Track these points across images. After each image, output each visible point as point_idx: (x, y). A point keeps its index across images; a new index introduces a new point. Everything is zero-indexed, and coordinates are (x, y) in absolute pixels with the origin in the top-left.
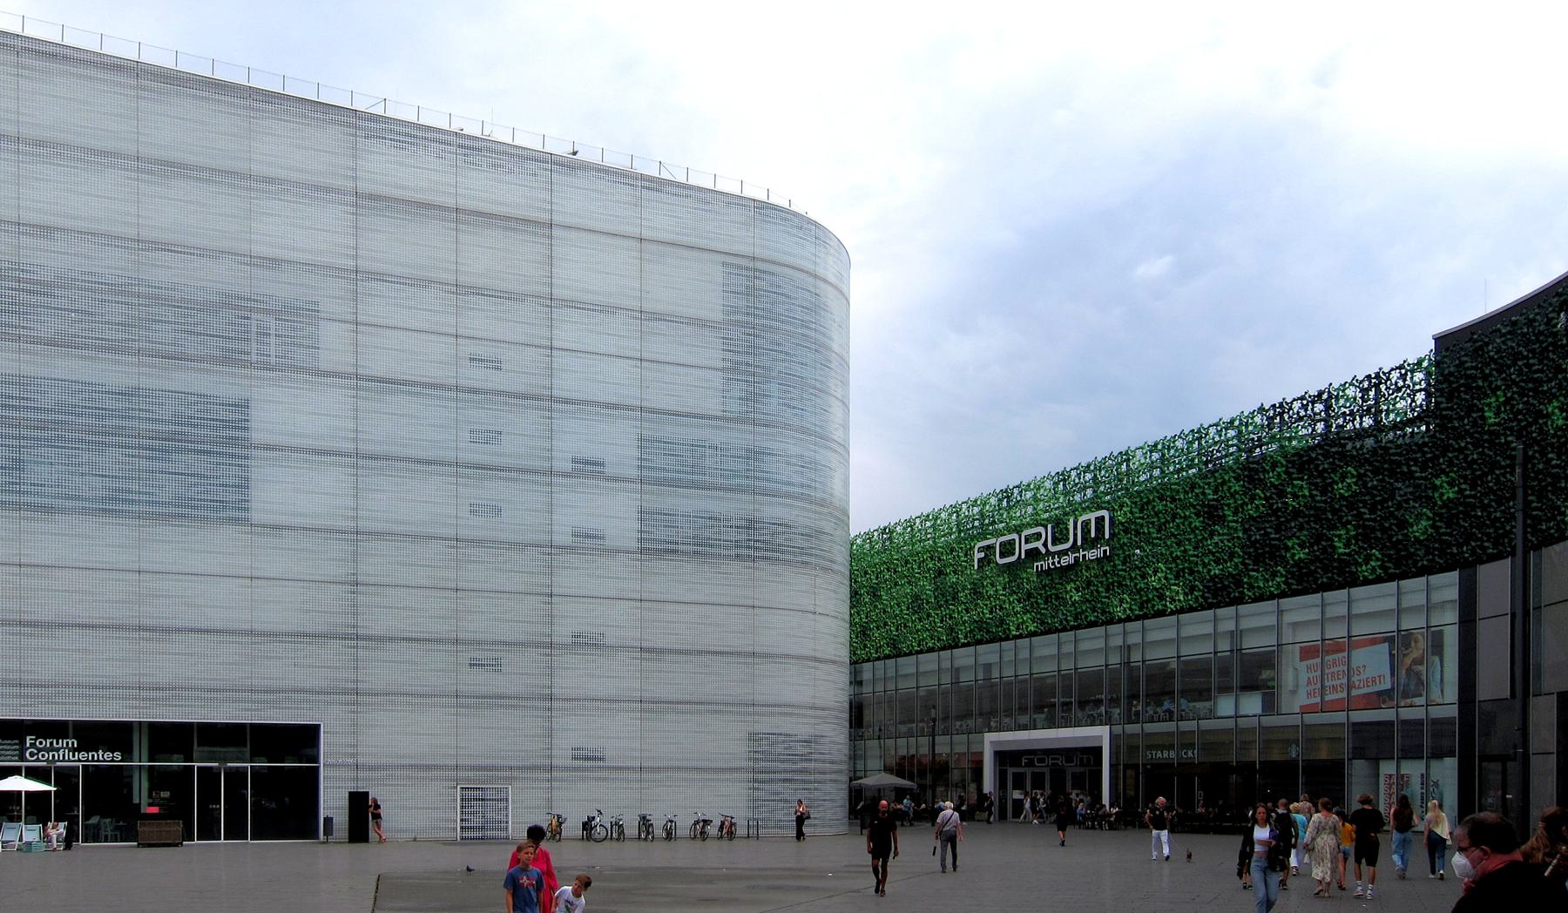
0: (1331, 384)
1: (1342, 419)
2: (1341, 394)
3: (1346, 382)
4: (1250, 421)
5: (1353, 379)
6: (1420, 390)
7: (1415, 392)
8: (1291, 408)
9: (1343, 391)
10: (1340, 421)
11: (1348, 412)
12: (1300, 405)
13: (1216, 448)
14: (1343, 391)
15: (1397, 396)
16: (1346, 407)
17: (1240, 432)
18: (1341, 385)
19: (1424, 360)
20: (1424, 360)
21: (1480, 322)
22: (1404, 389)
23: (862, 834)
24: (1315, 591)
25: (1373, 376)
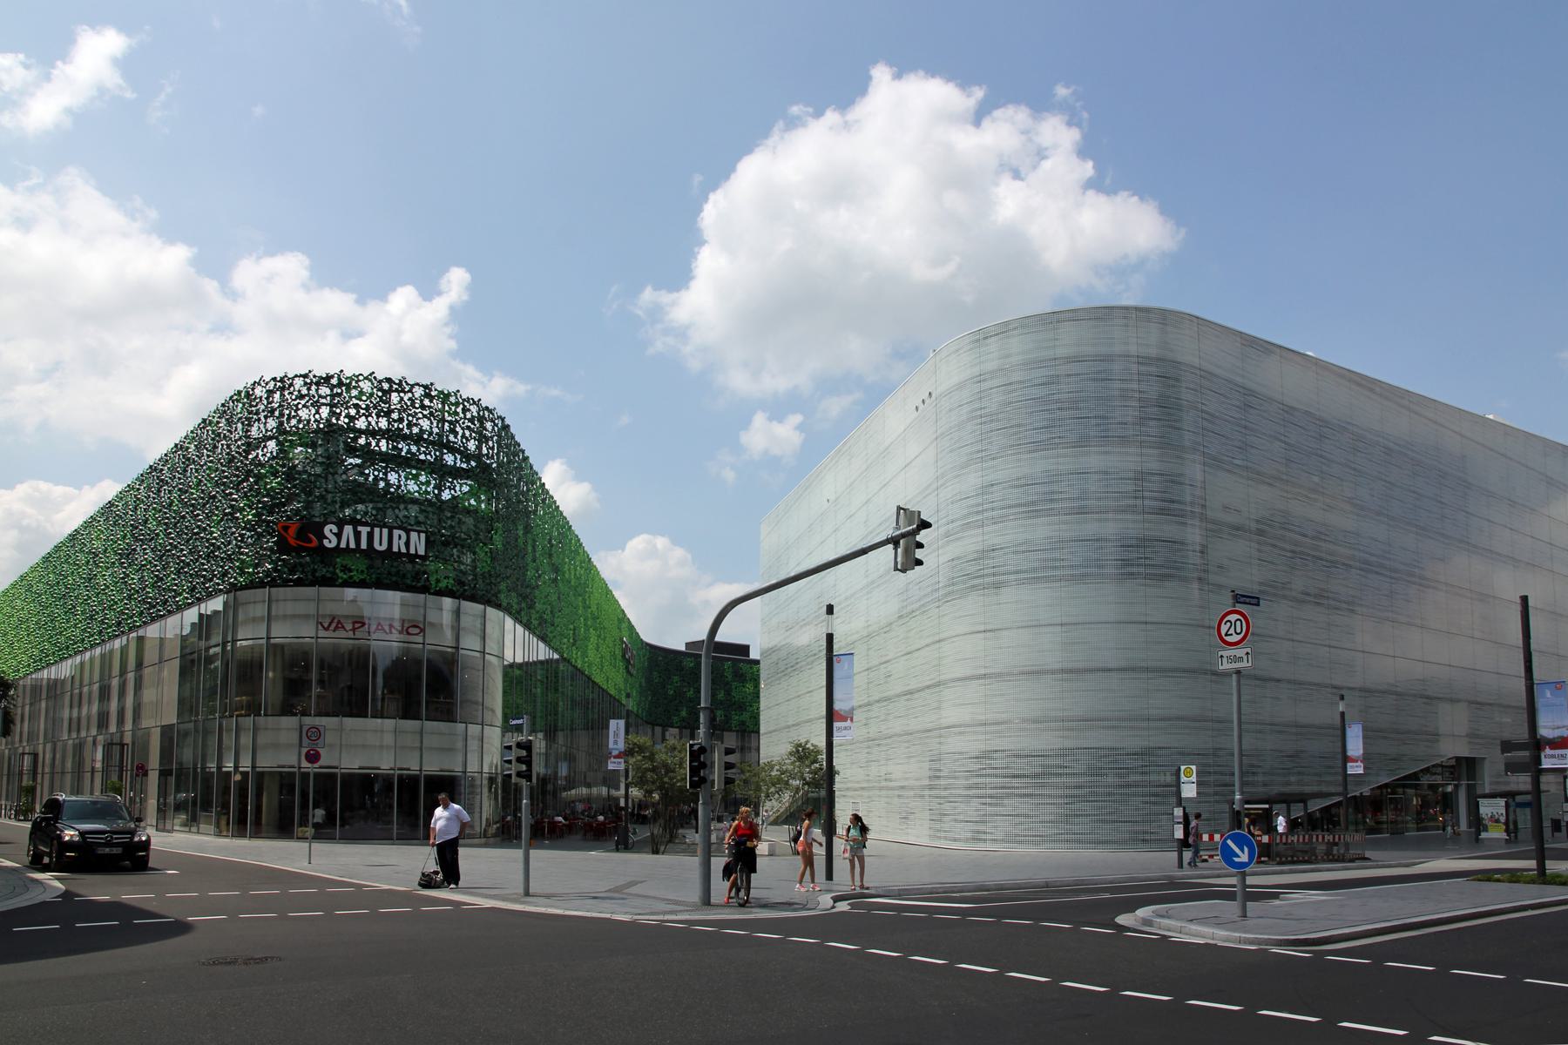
0: (373, 373)
4: (354, 384)
5: (371, 375)
8: (291, 385)
10: (353, 412)
12: (302, 383)
13: (303, 402)
18: (354, 375)
19: (332, 377)
20: (332, 377)
22: (307, 398)
24: (312, 584)
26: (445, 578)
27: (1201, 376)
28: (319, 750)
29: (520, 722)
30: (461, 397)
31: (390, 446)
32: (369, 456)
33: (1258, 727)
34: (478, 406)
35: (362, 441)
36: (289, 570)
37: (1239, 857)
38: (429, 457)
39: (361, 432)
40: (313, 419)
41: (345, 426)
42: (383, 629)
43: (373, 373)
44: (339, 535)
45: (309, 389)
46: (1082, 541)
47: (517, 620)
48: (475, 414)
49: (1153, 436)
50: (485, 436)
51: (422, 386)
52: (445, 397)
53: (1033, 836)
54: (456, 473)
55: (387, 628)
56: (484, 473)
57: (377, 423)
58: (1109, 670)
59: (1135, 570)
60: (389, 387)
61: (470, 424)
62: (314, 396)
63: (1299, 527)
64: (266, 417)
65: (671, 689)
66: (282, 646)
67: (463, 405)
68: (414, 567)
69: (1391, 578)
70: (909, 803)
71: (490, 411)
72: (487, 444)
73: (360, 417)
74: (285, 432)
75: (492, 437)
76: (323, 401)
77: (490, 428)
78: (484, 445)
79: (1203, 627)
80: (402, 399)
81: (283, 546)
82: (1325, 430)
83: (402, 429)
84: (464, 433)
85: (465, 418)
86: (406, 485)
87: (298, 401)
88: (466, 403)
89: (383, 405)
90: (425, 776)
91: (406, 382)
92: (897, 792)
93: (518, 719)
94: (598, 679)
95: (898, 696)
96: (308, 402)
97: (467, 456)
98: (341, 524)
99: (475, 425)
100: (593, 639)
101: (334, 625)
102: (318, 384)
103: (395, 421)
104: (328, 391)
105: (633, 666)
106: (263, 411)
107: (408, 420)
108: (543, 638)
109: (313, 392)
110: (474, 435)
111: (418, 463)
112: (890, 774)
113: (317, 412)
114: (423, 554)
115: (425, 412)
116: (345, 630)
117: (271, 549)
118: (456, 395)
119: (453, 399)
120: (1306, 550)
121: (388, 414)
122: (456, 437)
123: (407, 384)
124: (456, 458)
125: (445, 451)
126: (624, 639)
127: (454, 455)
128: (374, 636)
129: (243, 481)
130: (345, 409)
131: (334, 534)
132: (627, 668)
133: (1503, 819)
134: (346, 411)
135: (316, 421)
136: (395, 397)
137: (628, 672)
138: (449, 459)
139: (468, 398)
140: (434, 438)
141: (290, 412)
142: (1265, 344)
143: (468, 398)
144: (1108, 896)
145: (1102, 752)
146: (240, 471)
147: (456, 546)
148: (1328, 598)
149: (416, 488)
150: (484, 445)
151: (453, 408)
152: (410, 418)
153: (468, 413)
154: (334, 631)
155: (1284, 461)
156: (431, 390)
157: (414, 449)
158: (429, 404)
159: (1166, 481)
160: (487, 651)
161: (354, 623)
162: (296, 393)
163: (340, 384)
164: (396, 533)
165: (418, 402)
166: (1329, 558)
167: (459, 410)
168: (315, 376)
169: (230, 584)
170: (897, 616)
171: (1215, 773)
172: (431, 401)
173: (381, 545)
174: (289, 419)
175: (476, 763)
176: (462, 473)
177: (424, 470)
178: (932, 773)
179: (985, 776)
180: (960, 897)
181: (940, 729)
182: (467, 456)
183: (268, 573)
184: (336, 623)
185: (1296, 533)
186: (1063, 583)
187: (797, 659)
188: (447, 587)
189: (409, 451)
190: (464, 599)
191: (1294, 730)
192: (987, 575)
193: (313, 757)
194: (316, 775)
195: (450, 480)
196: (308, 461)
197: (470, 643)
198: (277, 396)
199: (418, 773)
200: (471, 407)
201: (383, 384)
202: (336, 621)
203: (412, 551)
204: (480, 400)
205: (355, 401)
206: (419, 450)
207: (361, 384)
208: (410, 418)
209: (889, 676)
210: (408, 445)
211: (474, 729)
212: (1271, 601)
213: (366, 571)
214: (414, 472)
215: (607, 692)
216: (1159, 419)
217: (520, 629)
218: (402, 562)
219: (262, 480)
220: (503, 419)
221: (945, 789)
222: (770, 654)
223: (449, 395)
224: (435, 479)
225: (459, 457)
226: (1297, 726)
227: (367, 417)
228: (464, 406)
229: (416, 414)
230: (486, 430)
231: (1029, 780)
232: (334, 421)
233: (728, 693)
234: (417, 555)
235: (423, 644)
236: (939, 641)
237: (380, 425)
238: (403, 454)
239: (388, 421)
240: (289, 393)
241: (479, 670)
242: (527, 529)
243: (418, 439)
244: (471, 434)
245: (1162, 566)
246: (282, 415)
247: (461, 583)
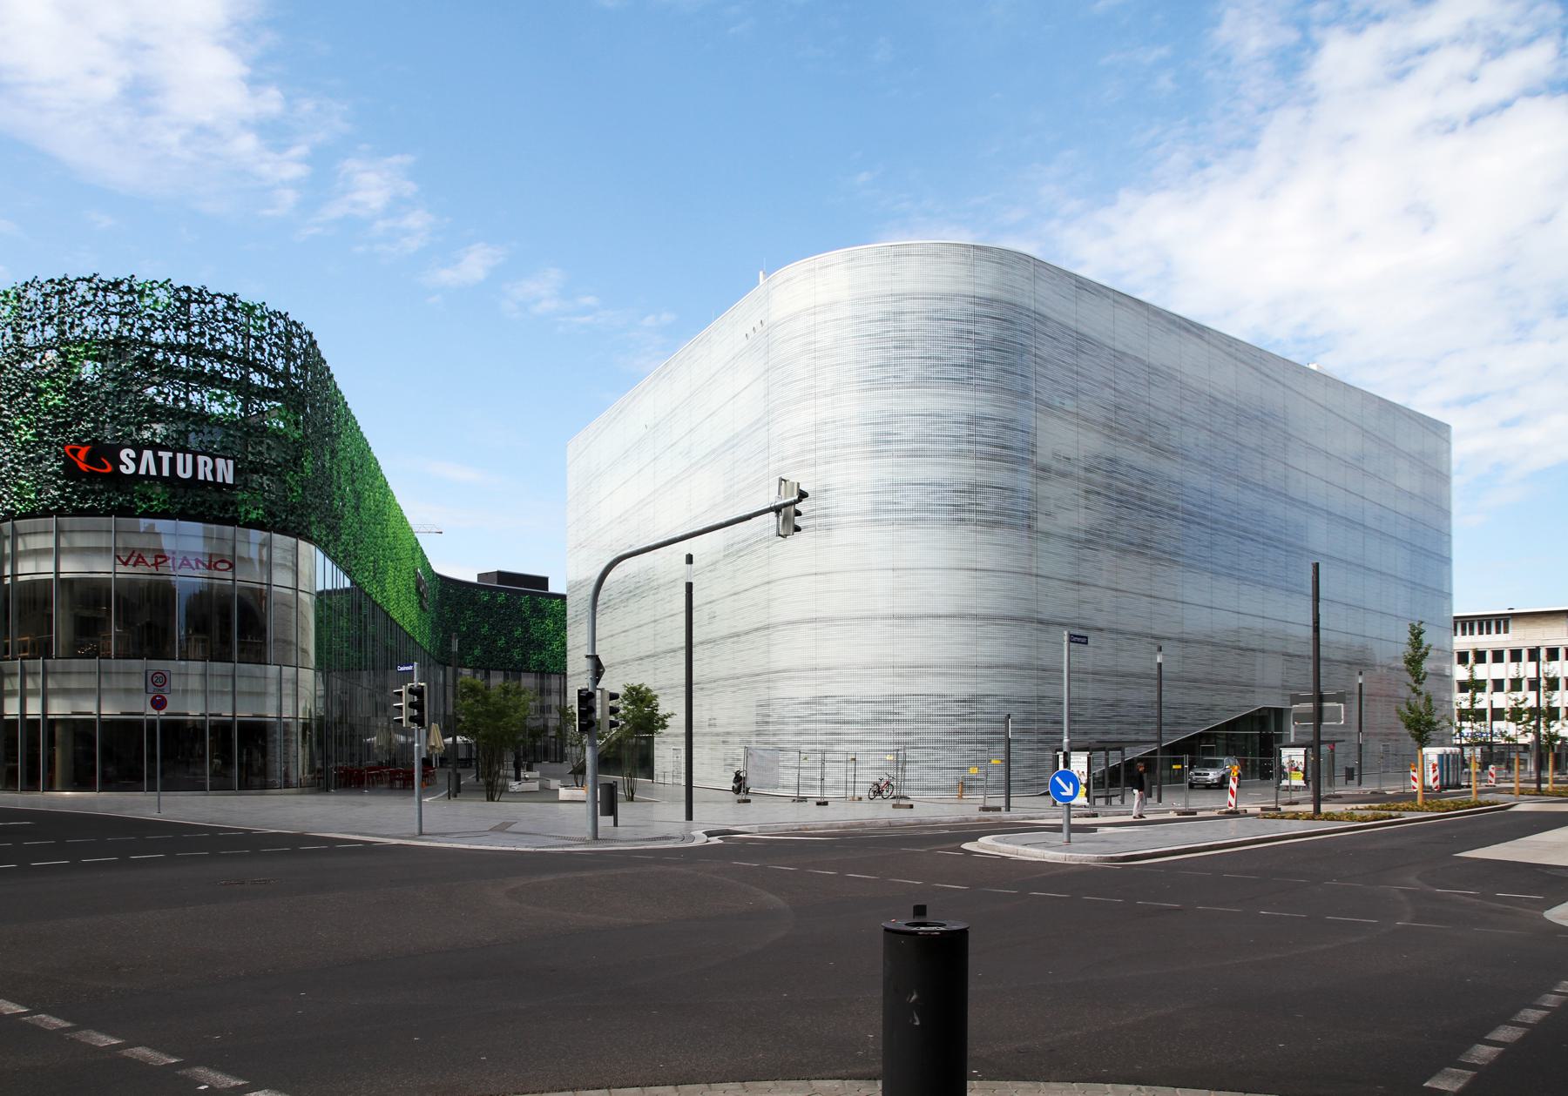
0: (169, 280)
1: (197, 331)
5: (166, 282)
10: (147, 323)
13: (88, 309)
15: (223, 326)
19: (122, 282)
21: (1335, 380)
22: (93, 306)
24: (108, 514)
26: (255, 509)
27: (1035, 319)
28: (166, 696)
29: (410, 668)
30: (267, 310)
31: (191, 363)
32: (170, 373)
33: (1081, 676)
34: (285, 321)
35: (159, 356)
36: (79, 497)
37: (1065, 791)
38: (234, 376)
39: (157, 346)
40: (101, 330)
41: (139, 339)
42: (189, 564)
43: (169, 280)
44: (137, 461)
45: (95, 295)
46: (915, 484)
47: (327, 554)
48: (282, 329)
49: (988, 380)
51: (225, 297)
52: (249, 310)
54: (264, 394)
55: (193, 563)
56: (292, 394)
57: (175, 336)
58: (939, 616)
59: (966, 515)
60: (186, 298)
61: (277, 340)
62: (101, 304)
63: (1126, 476)
64: (43, 324)
65: (464, 625)
66: (71, 581)
67: (270, 319)
68: (221, 496)
69: (1212, 529)
70: (735, 749)
71: (298, 327)
72: (295, 362)
73: (156, 329)
74: (67, 343)
75: (300, 355)
76: (113, 309)
77: (298, 345)
78: (292, 363)
79: (1031, 575)
80: (203, 311)
81: (70, 470)
82: (1154, 377)
83: (204, 344)
84: (271, 350)
85: (272, 333)
86: (209, 407)
87: (82, 308)
88: (272, 317)
89: (181, 317)
90: (239, 722)
91: (206, 291)
92: (721, 739)
93: (408, 665)
94: (395, 615)
95: (723, 638)
96: (94, 309)
97: (275, 376)
98: (139, 448)
99: (283, 341)
100: (391, 573)
101: (134, 559)
102: (105, 290)
103: (195, 335)
104: (117, 299)
105: (426, 599)
106: (39, 317)
107: (210, 334)
108: (348, 573)
109: (100, 299)
110: (281, 352)
111: (223, 383)
112: (715, 719)
113: (106, 322)
114: (232, 482)
115: (229, 327)
116: (147, 564)
117: (55, 474)
118: (261, 307)
119: (258, 312)
120: (1132, 500)
121: (187, 327)
122: (262, 354)
123: (209, 294)
124: (263, 378)
125: (251, 370)
126: (419, 571)
127: (261, 374)
128: (180, 572)
129: (17, 396)
131: (132, 459)
132: (420, 602)
133: (1301, 768)
135: (104, 332)
136: (194, 307)
137: (422, 607)
138: (256, 378)
139: (274, 311)
140: (239, 355)
141: (74, 321)
142: (1100, 289)
143: (274, 311)
144: (947, 831)
145: (931, 699)
146: (13, 384)
147: (265, 474)
148: (1151, 548)
149: (221, 410)
150: (292, 363)
151: (259, 322)
152: (213, 333)
153: (274, 328)
154: (134, 565)
155: (1113, 408)
156: (234, 301)
157: (218, 366)
158: (233, 317)
159: (998, 426)
161: (156, 557)
162: (79, 299)
163: (131, 291)
164: (201, 459)
165: (221, 314)
166: (1155, 508)
167: (266, 324)
168: (101, 281)
169: (7, 511)
170: (722, 554)
171: (1039, 721)
172: (235, 314)
173: (185, 472)
174: (72, 326)
175: (291, 708)
176: (271, 394)
177: (229, 390)
178: (760, 719)
179: (816, 721)
180: (825, 833)
181: (769, 673)
182: (275, 376)
183: (54, 502)
184: (136, 556)
185: (1122, 481)
186: (895, 527)
187: (610, 595)
188: (258, 518)
189: (213, 369)
190: (274, 532)
191: (1115, 679)
192: (819, 516)
193: (159, 704)
194: (162, 722)
195: (258, 401)
196: (97, 376)
197: (282, 578)
198: (55, 301)
199: (231, 719)
200: (278, 322)
201: (181, 293)
202: (136, 554)
203: (220, 480)
204: (287, 313)
205: (149, 311)
206: (223, 367)
208: (213, 333)
209: (715, 617)
210: (211, 362)
211: (288, 672)
212: (1097, 550)
213: (168, 501)
214: (219, 392)
215: (403, 629)
216: (994, 363)
217: (328, 562)
218: (208, 491)
219: (42, 396)
220: (310, 335)
221: (774, 735)
222: (579, 589)
223: (254, 308)
224: (241, 400)
225: (266, 376)
226: (1117, 676)
227: (164, 330)
228: (271, 320)
229: (220, 328)
230: (294, 347)
231: (859, 726)
232: (125, 333)
233: (526, 630)
234: (224, 484)
236: (768, 583)
237: (179, 338)
238: (206, 371)
239: (188, 335)
240: (72, 299)
241: (291, 608)
242: (333, 453)
243: (221, 356)
244: (279, 351)
245: (992, 513)
246: (63, 323)
247: (271, 514)
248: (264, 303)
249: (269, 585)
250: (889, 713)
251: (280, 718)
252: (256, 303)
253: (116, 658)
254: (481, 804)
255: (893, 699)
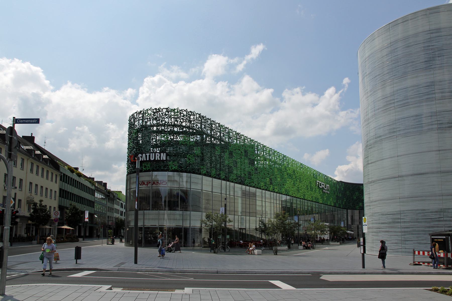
0: (151, 108)
2: (147, 112)
3: (148, 109)
5: (151, 108)
6: (141, 120)
7: (139, 120)
9: (147, 111)
10: (146, 120)
11: (149, 118)
14: (147, 111)
15: (165, 117)
16: (148, 116)
17: (143, 115)
18: (147, 109)
19: (142, 111)
23: (211, 252)
25: (158, 109)
34: (210, 121)
38: (168, 130)
42: (155, 184)
50: (230, 137)
51: (165, 108)
53: (419, 94)
55: (156, 183)
61: (208, 126)
71: (214, 122)
72: (231, 139)
90: (184, 228)
91: (160, 108)
110: (209, 129)
118: (177, 109)
119: (176, 111)
127: (177, 128)
130: (161, 127)
134: (161, 128)
138: (176, 129)
154: (143, 185)
156: (168, 109)
157: (163, 128)
160: (203, 189)
163: (178, 112)
173: (152, 158)
176: (180, 133)
189: (162, 129)
190: (214, 178)
199: (182, 227)
204: (211, 119)
206: (165, 128)
207: (165, 119)
214: (163, 135)
230: (213, 127)
235: (190, 188)
238: (160, 130)
248: (206, 116)
249: (202, 190)
250: (399, 219)
251: (250, 228)
252: (175, 108)
253: (151, 210)
254: (213, 254)
255: (400, 213)
